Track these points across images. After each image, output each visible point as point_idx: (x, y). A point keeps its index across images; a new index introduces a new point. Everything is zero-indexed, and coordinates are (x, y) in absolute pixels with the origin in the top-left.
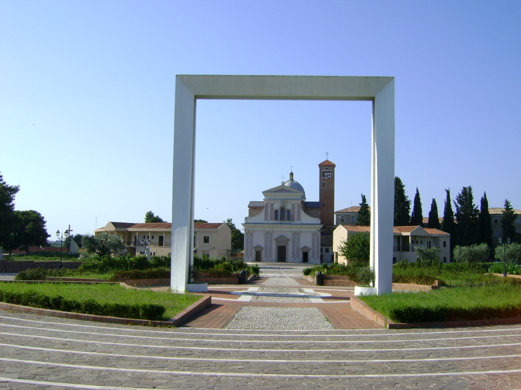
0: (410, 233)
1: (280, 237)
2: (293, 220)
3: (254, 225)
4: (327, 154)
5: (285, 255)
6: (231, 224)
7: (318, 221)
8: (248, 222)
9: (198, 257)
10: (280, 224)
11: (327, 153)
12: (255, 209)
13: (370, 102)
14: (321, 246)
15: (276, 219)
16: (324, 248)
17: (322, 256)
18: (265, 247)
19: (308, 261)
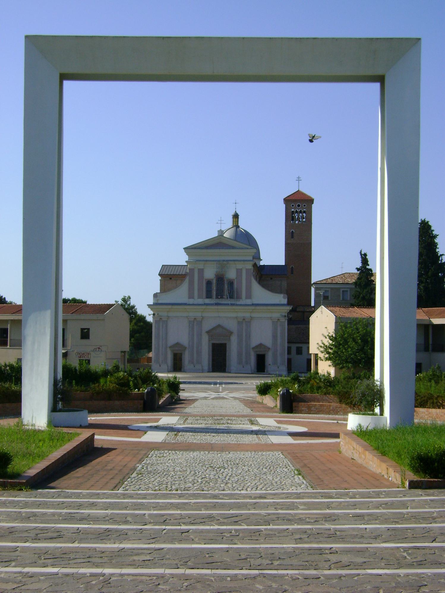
1: (214, 329)
2: (239, 297)
4: (299, 179)
5: (224, 360)
7: (283, 299)
8: (160, 302)
11: (299, 178)
12: (171, 279)
13: (377, 85)
14: (288, 343)
15: (209, 295)
16: (294, 347)
17: (289, 361)
18: (189, 346)
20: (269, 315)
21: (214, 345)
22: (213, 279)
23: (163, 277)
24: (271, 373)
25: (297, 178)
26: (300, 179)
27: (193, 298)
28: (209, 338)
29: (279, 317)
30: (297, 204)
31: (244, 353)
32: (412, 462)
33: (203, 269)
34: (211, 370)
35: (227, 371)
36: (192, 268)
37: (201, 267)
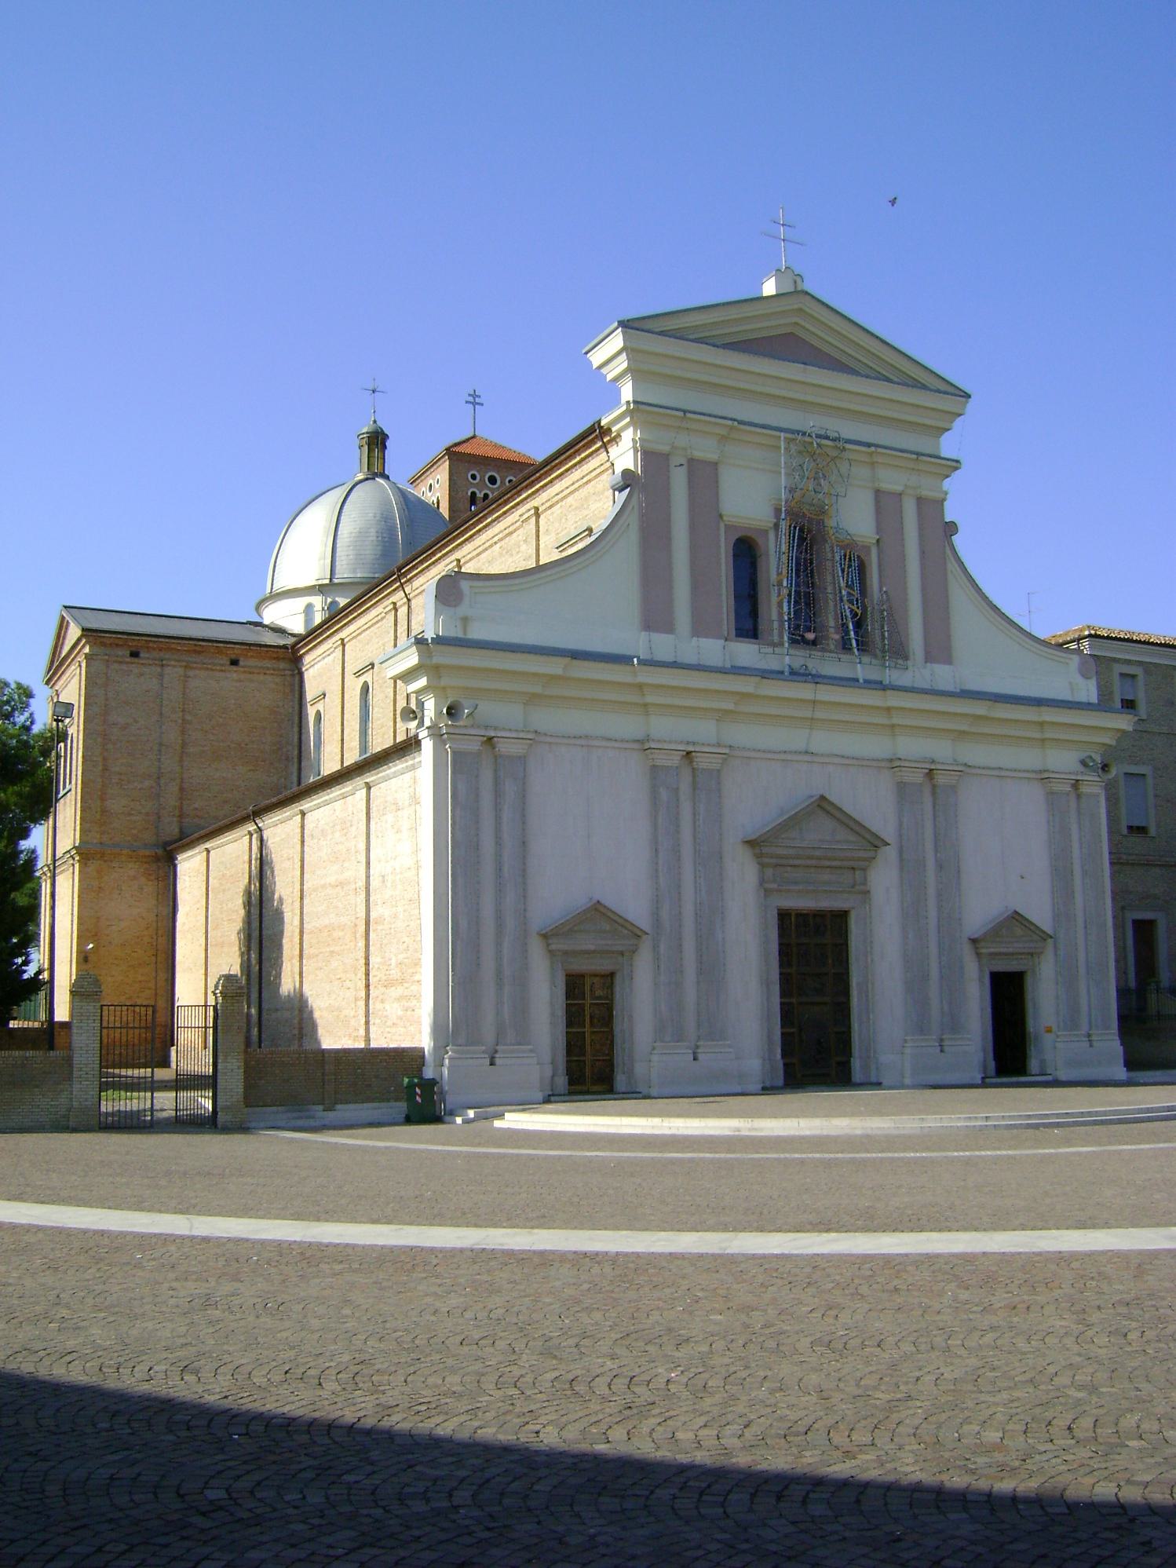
0: (423, 1040)
1: (794, 822)
2: (898, 652)
3: (555, 666)
5: (842, 1010)
6: (27, 729)
7: (1079, 680)
8: (476, 633)
9: (228, 978)
10: (797, 675)
11: (474, 395)
12: (135, 655)
15: (748, 625)
18: (657, 922)
19: (1033, 1065)
20: (1029, 758)
21: (783, 916)
22: (765, 532)
23: (103, 644)
24: (1063, 1075)
25: (470, 395)
26: (477, 400)
27: (668, 627)
28: (762, 882)
29: (1077, 774)
30: (487, 472)
31: (934, 973)
32: (607, 1269)
33: (715, 465)
34: (780, 1082)
35: (857, 1075)
36: (665, 449)
37: (705, 449)
